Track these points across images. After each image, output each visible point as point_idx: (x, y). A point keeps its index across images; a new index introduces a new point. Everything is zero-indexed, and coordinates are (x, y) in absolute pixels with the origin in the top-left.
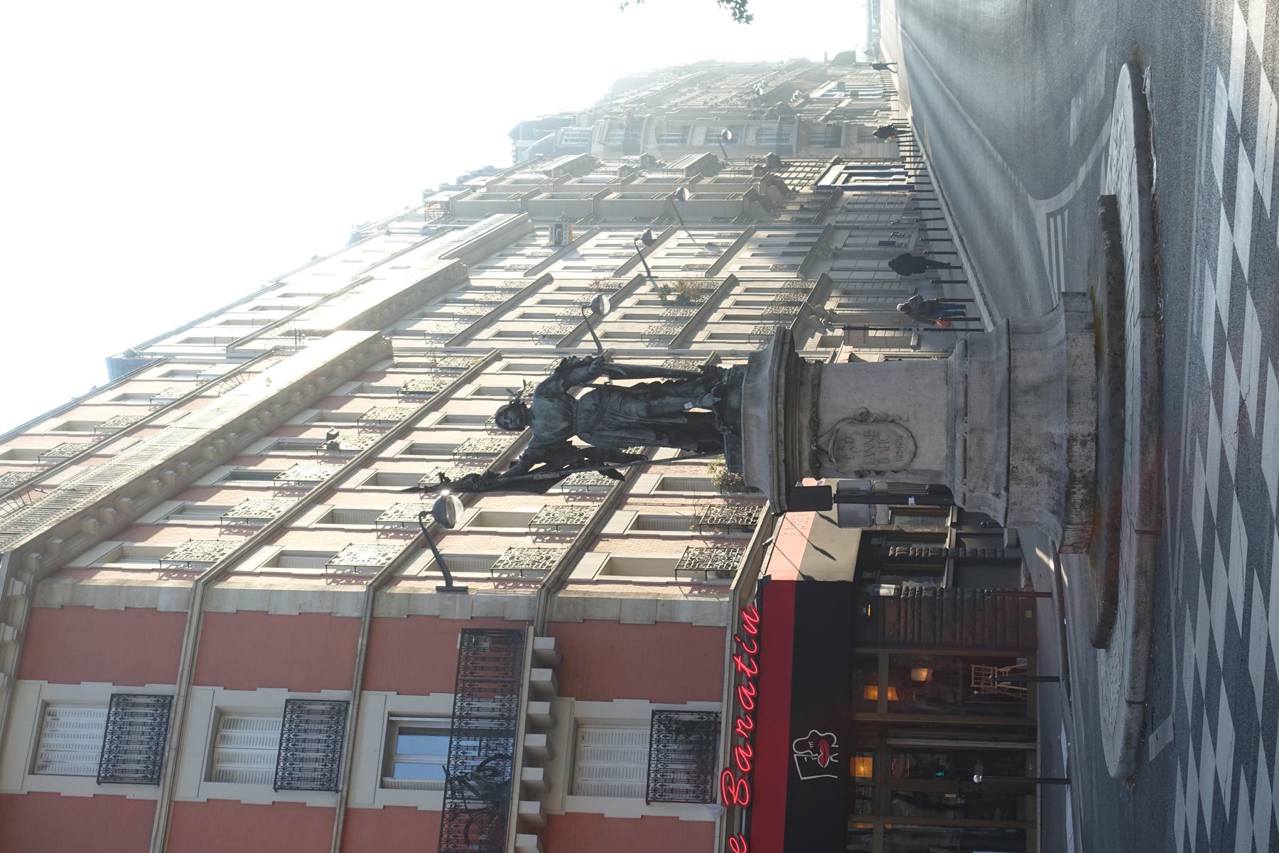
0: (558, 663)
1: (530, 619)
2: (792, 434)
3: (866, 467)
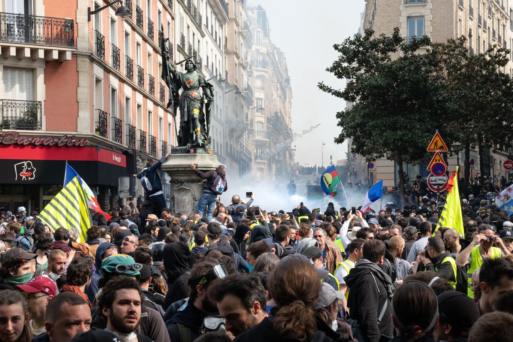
0: (60, 63)
3: (176, 200)
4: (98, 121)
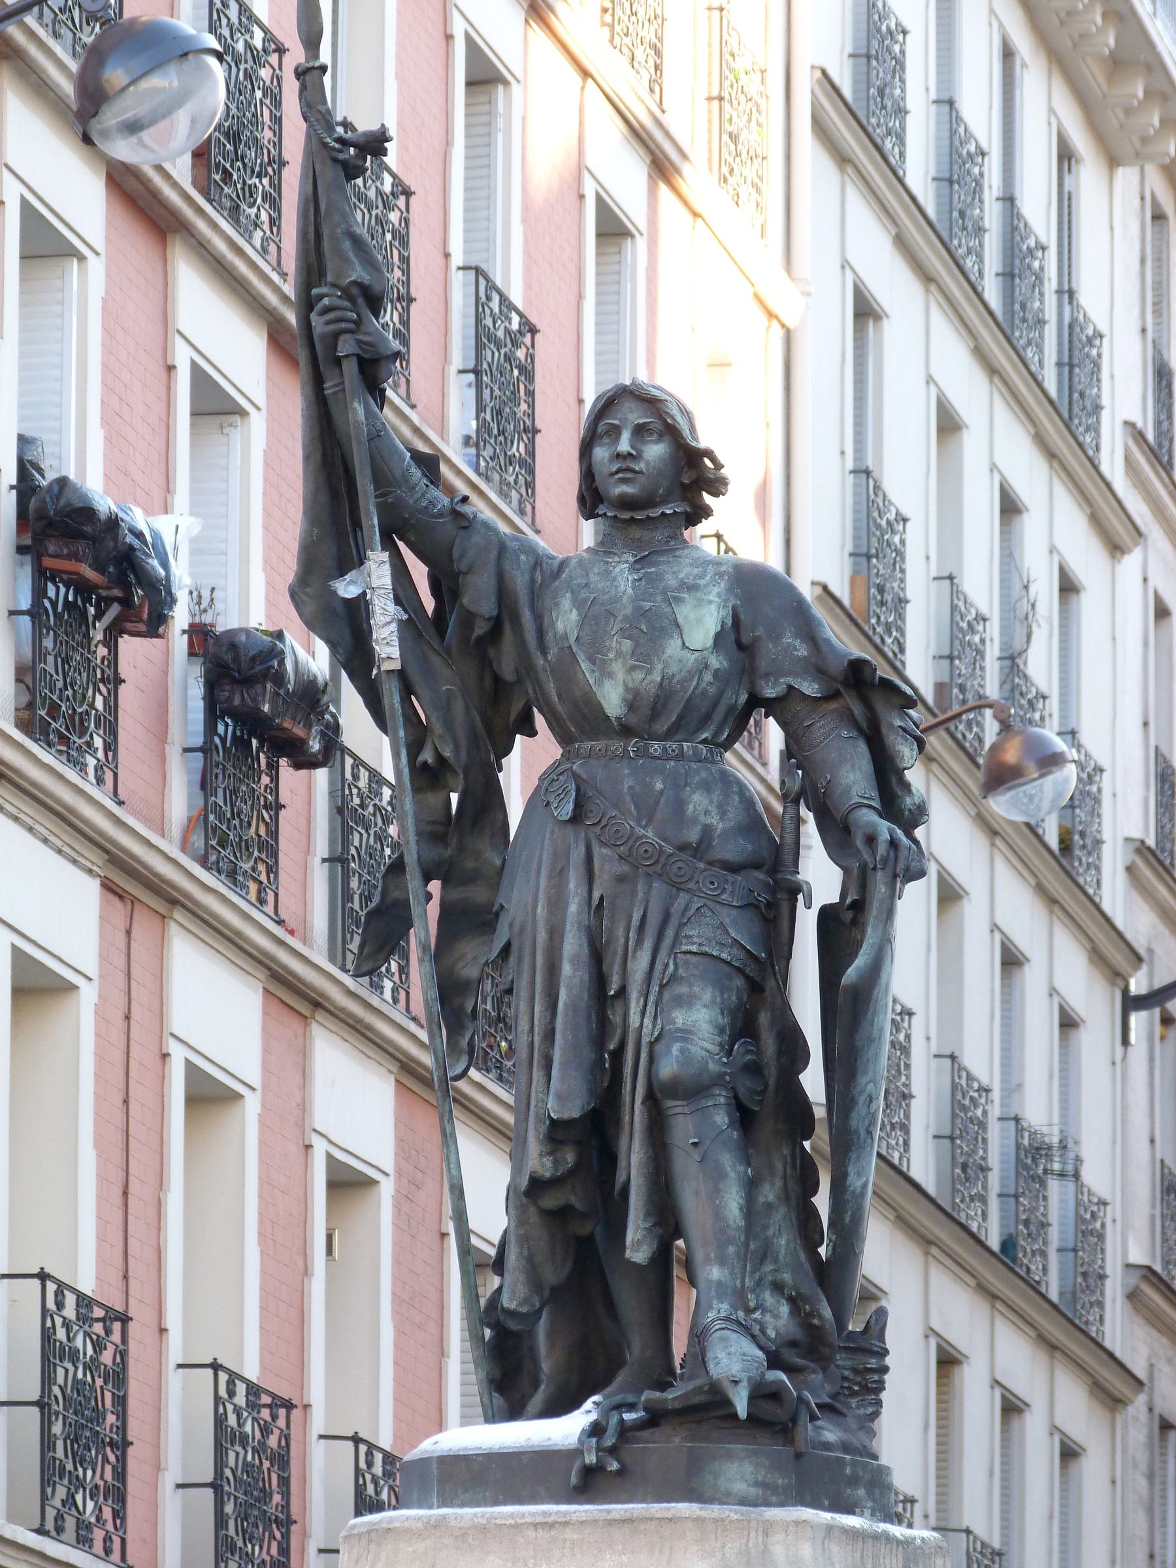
4: (209, 1477)
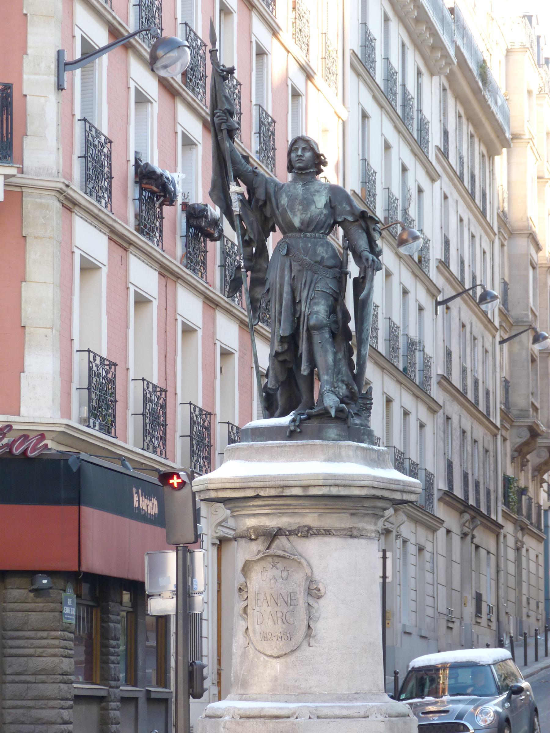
1: (25, 169)
2: (290, 505)
